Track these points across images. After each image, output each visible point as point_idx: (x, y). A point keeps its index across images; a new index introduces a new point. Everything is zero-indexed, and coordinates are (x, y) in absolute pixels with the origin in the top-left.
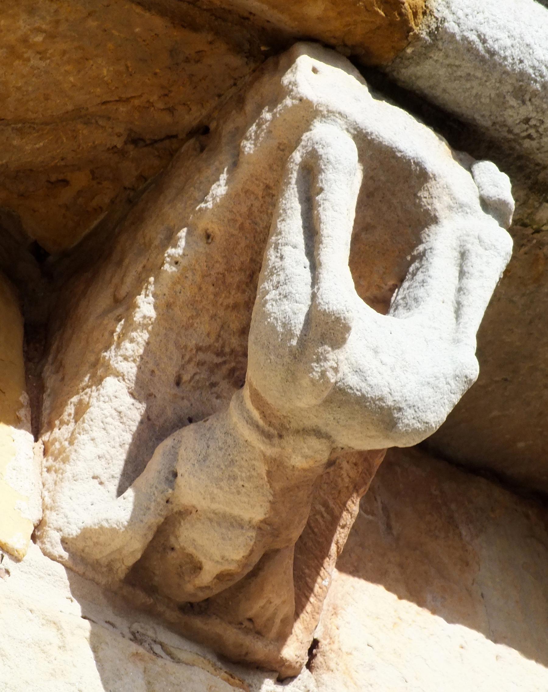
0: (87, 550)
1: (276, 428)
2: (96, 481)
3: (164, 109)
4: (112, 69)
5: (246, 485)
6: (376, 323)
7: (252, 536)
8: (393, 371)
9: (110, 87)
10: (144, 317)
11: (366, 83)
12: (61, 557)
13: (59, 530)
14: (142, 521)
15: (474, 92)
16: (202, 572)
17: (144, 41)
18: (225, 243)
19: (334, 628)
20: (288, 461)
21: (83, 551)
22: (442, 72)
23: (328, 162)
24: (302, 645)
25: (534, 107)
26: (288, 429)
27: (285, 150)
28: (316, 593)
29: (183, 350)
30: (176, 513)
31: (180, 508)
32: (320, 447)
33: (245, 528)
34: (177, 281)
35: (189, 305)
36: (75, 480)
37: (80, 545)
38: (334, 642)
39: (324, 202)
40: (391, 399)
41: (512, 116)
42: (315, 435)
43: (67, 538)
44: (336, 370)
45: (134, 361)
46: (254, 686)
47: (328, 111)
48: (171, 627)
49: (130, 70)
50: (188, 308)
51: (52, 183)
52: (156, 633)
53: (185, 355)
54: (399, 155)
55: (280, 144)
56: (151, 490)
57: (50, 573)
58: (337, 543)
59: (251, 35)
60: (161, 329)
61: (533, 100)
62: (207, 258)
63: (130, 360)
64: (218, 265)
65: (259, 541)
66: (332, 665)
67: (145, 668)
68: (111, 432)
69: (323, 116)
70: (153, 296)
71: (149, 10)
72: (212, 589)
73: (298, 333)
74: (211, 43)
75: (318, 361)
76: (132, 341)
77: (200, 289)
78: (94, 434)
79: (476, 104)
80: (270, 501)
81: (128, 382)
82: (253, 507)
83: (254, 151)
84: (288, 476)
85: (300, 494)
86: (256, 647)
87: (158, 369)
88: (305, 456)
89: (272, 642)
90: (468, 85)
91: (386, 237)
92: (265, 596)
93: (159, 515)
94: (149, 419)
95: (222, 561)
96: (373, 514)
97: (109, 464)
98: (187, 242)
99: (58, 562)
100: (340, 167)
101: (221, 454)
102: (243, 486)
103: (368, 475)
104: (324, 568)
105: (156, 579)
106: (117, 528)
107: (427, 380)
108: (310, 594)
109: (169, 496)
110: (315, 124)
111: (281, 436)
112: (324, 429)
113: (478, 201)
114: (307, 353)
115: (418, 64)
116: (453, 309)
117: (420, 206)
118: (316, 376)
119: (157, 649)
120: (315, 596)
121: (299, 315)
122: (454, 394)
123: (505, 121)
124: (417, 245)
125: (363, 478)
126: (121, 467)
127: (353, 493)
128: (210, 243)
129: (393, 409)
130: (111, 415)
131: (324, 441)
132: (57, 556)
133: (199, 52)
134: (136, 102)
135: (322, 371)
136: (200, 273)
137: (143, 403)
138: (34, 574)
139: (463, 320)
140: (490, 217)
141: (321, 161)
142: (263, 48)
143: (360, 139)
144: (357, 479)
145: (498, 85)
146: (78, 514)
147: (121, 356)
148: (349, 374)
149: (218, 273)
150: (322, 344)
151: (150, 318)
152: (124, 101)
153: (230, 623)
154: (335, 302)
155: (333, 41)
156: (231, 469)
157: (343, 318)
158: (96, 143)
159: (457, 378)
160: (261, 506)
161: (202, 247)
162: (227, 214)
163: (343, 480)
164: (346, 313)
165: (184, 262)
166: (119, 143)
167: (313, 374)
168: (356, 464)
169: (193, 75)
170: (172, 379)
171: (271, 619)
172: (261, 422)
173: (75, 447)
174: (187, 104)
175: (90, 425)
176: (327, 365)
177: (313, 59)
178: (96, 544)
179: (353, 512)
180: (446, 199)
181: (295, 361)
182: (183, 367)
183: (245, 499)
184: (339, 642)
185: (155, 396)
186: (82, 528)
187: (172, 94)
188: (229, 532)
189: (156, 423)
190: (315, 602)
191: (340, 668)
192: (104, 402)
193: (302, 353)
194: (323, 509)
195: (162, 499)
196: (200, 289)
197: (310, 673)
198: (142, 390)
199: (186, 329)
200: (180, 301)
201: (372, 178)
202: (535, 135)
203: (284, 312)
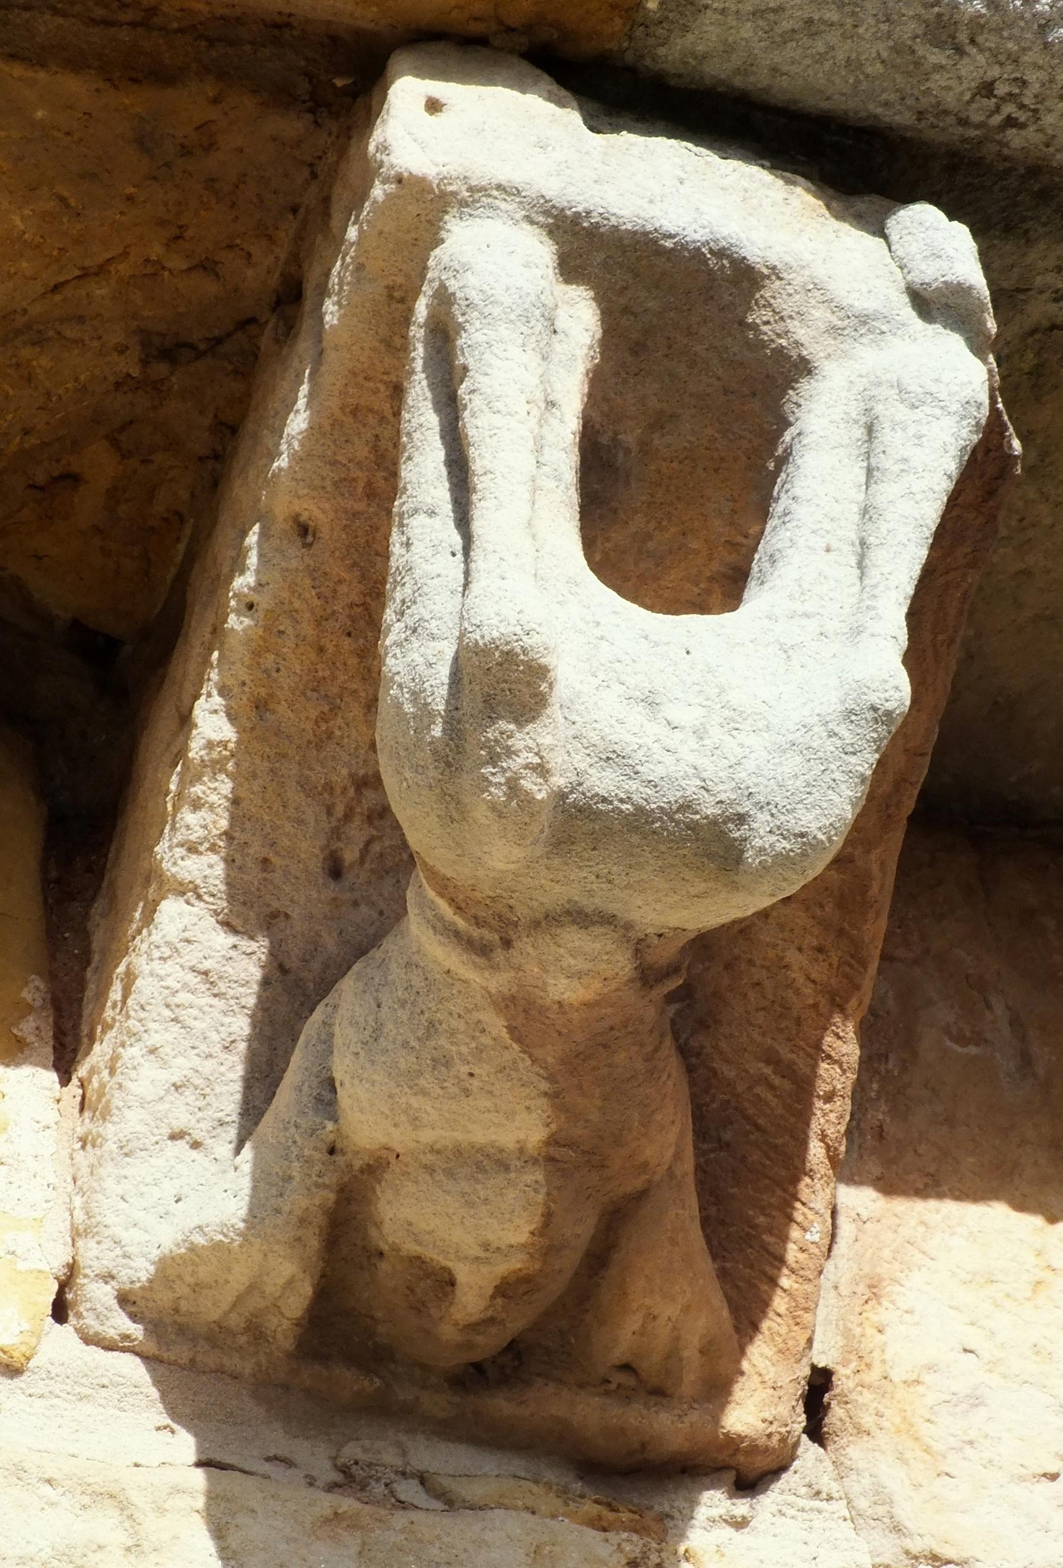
0: (184, 1305)
1: (492, 929)
2: (182, 1145)
3: (189, 269)
4: (27, 212)
5: (476, 1071)
6: (646, 638)
7: (536, 1182)
8: (701, 738)
9: (46, 252)
10: (210, 745)
11: (575, 104)
12: (126, 1337)
13: (108, 1277)
14: (278, 1211)
15: (841, 56)
16: (459, 1292)
17: (68, 134)
18: (344, 536)
19: (870, 1331)
20: (542, 994)
21: (177, 1310)
22: (747, 31)
23: (468, 306)
24: (776, 1393)
25: (987, 54)
26: (516, 925)
27: (400, 298)
28: (794, 1265)
29: (326, 795)
30: (362, 1171)
31: (366, 1159)
32: (597, 946)
33: (512, 1167)
34: (260, 648)
35: (309, 693)
36: (126, 1155)
37: (164, 1298)
38: (868, 1366)
39: (472, 396)
40: (711, 800)
41: (949, 88)
42: (574, 922)
43: (131, 1291)
44: (542, 770)
45: (213, 849)
46: (677, 1514)
47: (471, 189)
48: (447, 1430)
49: (73, 203)
50: (308, 699)
51: (42, 489)
52: (404, 1453)
53: (334, 804)
54: (669, 244)
55: (390, 288)
56: (287, 1134)
57: (105, 1382)
58: (823, 1137)
59: (307, 59)
60: (258, 761)
61: (980, 39)
62: (314, 579)
63: (202, 849)
64: (343, 589)
65: (559, 1188)
66: (867, 1420)
67: (364, 1543)
68: (190, 1022)
69: (463, 204)
70: (221, 694)
71: (43, 65)
72: (502, 1322)
73: (441, 707)
74: (215, 101)
75: (493, 759)
76: (197, 805)
77: (321, 650)
78: (154, 1039)
79: (858, 81)
80: (546, 1094)
81: (211, 900)
82: (510, 1115)
83: (338, 319)
84: (558, 1028)
85: (621, 1057)
86: (656, 1426)
87: (277, 853)
88: (576, 974)
89: (696, 1406)
90: (820, 46)
91: (709, 431)
92: (635, 1305)
93: (317, 1185)
94: (283, 970)
95: (488, 1255)
96: (979, 1039)
97: (204, 1096)
98: (261, 556)
99: (124, 1350)
100: (496, 311)
101: (403, 1014)
102: (471, 1075)
103: (856, 965)
104: (804, 1204)
105: (381, 1329)
106: (227, 1241)
107: (791, 737)
108: (779, 1269)
109: (332, 1137)
110: (448, 226)
111: (507, 944)
112: (589, 904)
113: (906, 299)
114: (468, 748)
115: (685, 29)
116: (853, 560)
117: (763, 345)
118: (499, 794)
119: (408, 1490)
120: (793, 1271)
121: (438, 667)
122: (854, 754)
123: (939, 103)
124: (780, 433)
125: (846, 976)
126: (238, 1097)
127: (831, 1016)
128: (311, 545)
129: (725, 823)
130: (185, 985)
131: (599, 930)
132: (116, 1337)
133: (201, 126)
134: (123, 268)
135: (508, 781)
136: (308, 615)
137: (260, 938)
138: (64, 1395)
139: (874, 575)
140: (938, 327)
141: (456, 306)
142: (339, 83)
143: (565, 232)
144: (833, 981)
145: (884, 27)
146: (146, 1231)
147: (181, 845)
148: (591, 771)
149: (351, 606)
150: (493, 720)
151: (224, 744)
152: (96, 274)
153: (581, 1386)
154: (494, 621)
155: (476, 28)
156: (433, 1043)
157: (518, 650)
158: (82, 378)
159: (853, 718)
160: (528, 1108)
161: (295, 557)
162: (326, 471)
163: (797, 992)
164: (525, 638)
165: (264, 602)
166: (129, 365)
167: (491, 794)
168: (820, 950)
169: (213, 180)
170: (316, 866)
171: (673, 1354)
172: (461, 923)
173: (118, 1078)
174: (237, 245)
175: (140, 1021)
176: (515, 764)
177: (427, 81)
178: (197, 1288)
179: (844, 1059)
180: (820, 315)
181: (451, 772)
182: (336, 833)
183: (485, 1103)
184: (883, 1361)
185: (287, 916)
186: (157, 1259)
187: (189, 233)
188: (479, 1187)
189: (304, 974)
190: (796, 1286)
191: (886, 1424)
192: (162, 959)
193: (459, 750)
194: (768, 1071)
195: (315, 1149)
196: (321, 650)
197: (821, 1450)
198: (248, 908)
199: (319, 748)
200: (282, 688)
201: (626, 310)
202: (1022, 116)
203: (412, 666)
